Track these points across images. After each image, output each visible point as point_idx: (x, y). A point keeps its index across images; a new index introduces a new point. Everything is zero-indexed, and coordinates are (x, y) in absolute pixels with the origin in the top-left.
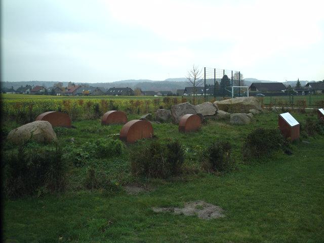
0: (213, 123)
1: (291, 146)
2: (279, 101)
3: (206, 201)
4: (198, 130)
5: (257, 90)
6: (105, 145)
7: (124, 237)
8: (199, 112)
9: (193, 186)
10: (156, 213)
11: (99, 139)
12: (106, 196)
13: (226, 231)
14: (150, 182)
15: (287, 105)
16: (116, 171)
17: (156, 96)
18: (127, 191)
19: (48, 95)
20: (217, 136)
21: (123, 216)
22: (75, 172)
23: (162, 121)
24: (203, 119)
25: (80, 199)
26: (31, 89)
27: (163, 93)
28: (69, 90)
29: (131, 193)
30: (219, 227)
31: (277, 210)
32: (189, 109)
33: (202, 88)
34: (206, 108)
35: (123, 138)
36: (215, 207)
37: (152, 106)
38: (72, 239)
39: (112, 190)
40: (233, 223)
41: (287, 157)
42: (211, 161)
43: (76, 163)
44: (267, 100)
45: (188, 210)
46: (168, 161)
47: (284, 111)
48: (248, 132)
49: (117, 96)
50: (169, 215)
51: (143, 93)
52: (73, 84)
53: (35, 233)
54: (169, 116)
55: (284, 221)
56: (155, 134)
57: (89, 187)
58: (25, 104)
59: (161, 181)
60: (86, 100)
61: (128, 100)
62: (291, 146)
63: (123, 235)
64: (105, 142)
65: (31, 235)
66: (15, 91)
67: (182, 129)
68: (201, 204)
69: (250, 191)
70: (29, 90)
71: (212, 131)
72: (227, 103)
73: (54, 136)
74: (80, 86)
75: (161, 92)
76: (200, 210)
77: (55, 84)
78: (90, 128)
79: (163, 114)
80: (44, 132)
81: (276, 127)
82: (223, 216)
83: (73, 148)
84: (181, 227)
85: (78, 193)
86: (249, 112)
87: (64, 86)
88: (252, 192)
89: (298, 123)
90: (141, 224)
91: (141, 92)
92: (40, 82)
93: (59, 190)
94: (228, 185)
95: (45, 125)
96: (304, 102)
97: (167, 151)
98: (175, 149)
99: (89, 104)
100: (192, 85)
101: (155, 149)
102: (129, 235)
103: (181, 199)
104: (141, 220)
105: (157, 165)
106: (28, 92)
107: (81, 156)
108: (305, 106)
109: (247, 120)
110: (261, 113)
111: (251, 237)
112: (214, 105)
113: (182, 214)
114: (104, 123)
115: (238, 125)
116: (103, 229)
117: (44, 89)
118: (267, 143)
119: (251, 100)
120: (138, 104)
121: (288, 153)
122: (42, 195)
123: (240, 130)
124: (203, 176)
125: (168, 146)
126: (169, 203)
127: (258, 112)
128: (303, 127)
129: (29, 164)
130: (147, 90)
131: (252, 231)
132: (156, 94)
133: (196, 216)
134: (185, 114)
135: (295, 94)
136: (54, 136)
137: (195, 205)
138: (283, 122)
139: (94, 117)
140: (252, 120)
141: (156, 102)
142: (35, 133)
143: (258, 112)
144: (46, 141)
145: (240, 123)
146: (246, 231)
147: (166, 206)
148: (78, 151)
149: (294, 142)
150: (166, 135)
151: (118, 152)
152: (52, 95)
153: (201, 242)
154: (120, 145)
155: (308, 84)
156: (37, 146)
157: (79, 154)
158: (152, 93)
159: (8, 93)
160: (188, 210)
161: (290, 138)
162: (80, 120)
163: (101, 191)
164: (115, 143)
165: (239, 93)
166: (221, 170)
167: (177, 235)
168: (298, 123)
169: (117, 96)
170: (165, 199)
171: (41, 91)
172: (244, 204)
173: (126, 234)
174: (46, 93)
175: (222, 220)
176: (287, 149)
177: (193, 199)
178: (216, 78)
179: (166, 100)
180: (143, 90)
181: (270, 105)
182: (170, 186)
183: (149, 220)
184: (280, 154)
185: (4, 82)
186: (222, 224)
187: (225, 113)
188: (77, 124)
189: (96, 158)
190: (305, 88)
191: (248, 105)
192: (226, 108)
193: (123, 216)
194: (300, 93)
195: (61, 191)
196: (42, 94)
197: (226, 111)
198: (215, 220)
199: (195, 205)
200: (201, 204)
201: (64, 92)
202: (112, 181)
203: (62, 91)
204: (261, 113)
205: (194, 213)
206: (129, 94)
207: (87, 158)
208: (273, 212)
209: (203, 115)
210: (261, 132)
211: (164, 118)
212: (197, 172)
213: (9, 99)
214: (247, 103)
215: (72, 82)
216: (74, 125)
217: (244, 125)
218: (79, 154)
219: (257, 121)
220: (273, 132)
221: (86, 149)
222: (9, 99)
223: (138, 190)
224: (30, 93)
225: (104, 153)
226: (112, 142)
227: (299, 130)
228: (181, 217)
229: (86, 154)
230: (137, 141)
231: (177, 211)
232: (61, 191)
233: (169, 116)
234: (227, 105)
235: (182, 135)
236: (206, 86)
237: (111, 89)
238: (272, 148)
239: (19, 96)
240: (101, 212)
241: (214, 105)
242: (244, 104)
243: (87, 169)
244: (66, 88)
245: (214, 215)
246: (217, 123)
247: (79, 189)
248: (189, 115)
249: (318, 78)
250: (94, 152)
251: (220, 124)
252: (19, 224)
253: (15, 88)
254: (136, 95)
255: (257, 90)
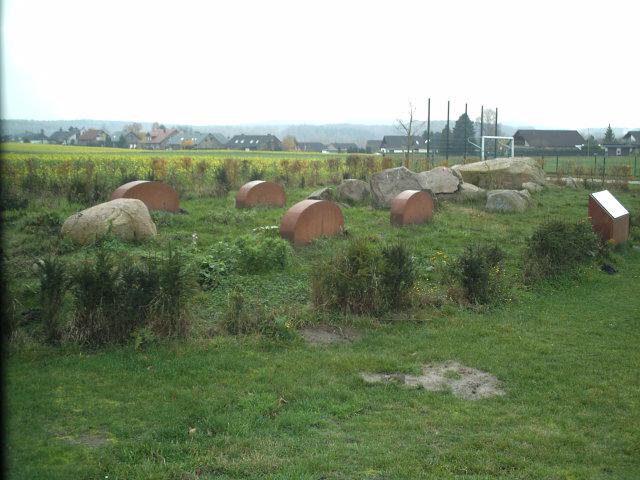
0: (453, 208)
1: (614, 256)
2: (576, 166)
3: (465, 362)
4: (427, 221)
5: (527, 145)
6: (255, 248)
7: (314, 429)
8: (426, 186)
9: (434, 332)
10: (370, 385)
11: (243, 237)
12: (267, 348)
13: (511, 423)
14: (350, 322)
15: (592, 174)
16: (283, 300)
17: (324, 152)
18: (306, 339)
19: (112, 147)
20: (467, 234)
21: (305, 388)
22: (201, 300)
23: (351, 202)
24: (435, 200)
25: (217, 353)
26: (78, 135)
27: (339, 147)
28: (153, 138)
29: (314, 344)
30: (497, 415)
31: (605, 383)
32: (408, 181)
33: (418, 138)
34: (441, 176)
35: (286, 234)
36: (483, 375)
37: (324, 172)
38: (214, 433)
39: (277, 338)
40: (523, 408)
41: (605, 277)
42: (466, 283)
43: (201, 283)
44: (551, 163)
45: (431, 379)
46: (385, 282)
47: (599, 188)
48: (529, 230)
49: (247, 150)
50: (396, 389)
51: (301, 146)
52: (162, 127)
53: (142, 419)
54: (366, 194)
55: (621, 406)
56: (348, 227)
57: (232, 330)
58: (78, 165)
59: (372, 320)
60: (196, 159)
61: (279, 160)
62: (614, 256)
63: (312, 425)
64: (255, 241)
65: (135, 422)
66: (46, 138)
67: (397, 219)
68: (454, 367)
69: (548, 345)
70: (74, 137)
71: (455, 224)
72: (478, 169)
73: (152, 229)
74: (176, 132)
75: (335, 145)
76: (452, 379)
77: (126, 126)
78: (218, 214)
79: (353, 189)
80: (133, 220)
81: (583, 216)
82: (501, 393)
83: (197, 255)
84: (423, 412)
85: (213, 341)
86: (521, 189)
87: (144, 130)
88: (551, 345)
89: (627, 212)
90: (346, 406)
91: (297, 144)
92: (97, 121)
93: (175, 335)
94: (503, 331)
95: (135, 207)
96: (626, 170)
97: (382, 263)
98: (397, 257)
99: (202, 167)
100: (406, 133)
101: (357, 259)
102: (324, 426)
103: (415, 357)
104: (343, 399)
105: (363, 289)
106: (73, 141)
107: (211, 269)
108: (628, 177)
109: (521, 204)
110: (545, 190)
111: (564, 436)
112: (454, 173)
113: (420, 388)
114: (241, 204)
115: (503, 213)
116: (271, 413)
117: (104, 136)
118: (570, 251)
119: (527, 164)
120: (297, 167)
121: (607, 269)
122: (145, 345)
123: (507, 222)
124: (450, 313)
125: (383, 253)
126: (392, 365)
127: (539, 188)
128: (633, 219)
129: (117, 283)
130: (308, 141)
131: (563, 425)
132: (326, 148)
133: (448, 392)
134: (403, 189)
135: (602, 153)
136: (152, 229)
137: (444, 370)
138: (596, 208)
139: (217, 192)
140: (529, 205)
141: (333, 164)
142: (116, 222)
143: (539, 188)
144: (137, 239)
145: (506, 208)
146: (552, 425)
147: (387, 372)
148: (204, 258)
149: (618, 249)
150: (375, 235)
151: (280, 262)
152: (107, 146)
153: (122, 477)
154: (284, 248)
155: (629, 135)
156: (122, 247)
157: (207, 265)
158: (317, 147)
159: (33, 142)
160: (431, 379)
161: (611, 240)
162: (190, 198)
163: (256, 338)
164: (275, 245)
165: (494, 151)
166: (484, 301)
167: (417, 428)
168: (627, 212)
169: (247, 150)
170: (383, 356)
171: (98, 139)
172: (538, 370)
173: (318, 425)
174: (108, 143)
175: (500, 401)
176: (607, 262)
177: (439, 359)
178: (431, 120)
179: (352, 161)
180: (299, 141)
181: (559, 174)
182: (388, 332)
183: (358, 398)
184: (593, 271)
185: (10, 121)
186: (502, 409)
187: (475, 189)
188: (188, 206)
189: (240, 273)
190: (623, 141)
191: (519, 175)
192: (475, 178)
193: (305, 388)
194: (612, 150)
195: (179, 337)
196: (100, 144)
197: (476, 183)
198: (487, 401)
199: (444, 370)
200: (454, 367)
201: (144, 141)
202: (278, 320)
203: (140, 139)
204: (545, 190)
205: (444, 386)
206: (273, 146)
207: (222, 273)
208: (598, 387)
209: (435, 191)
210: (559, 228)
211: (355, 197)
212: (438, 304)
213: (17, 152)
214: (517, 170)
215: (160, 123)
216: (181, 206)
217: (514, 213)
218: (207, 265)
219: (540, 205)
220: (579, 228)
221: (219, 256)
222: (17, 152)
223: (327, 338)
224: (76, 142)
225: (253, 265)
226: (269, 244)
227: (627, 226)
228: (419, 393)
229: (221, 266)
230: (314, 243)
231: (410, 381)
232: (179, 337)
233: (366, 194)
234: (477, 172)
235: (397, 231)
236: (427, 135)
237: (236, 137)
238: (578, 259)
239: (54, 147)
240: (261, 380)
241: (454, 173)
242: (511, 171)
243: (230, 294)
244: (148, 135)
245: (484, 391)
246: (462, 209)
247: (212, 334)
248: (411, 192)
249: (624, 124)
250: (234, 260)
251: (467, 210)
252: (107, 401)
253: (48, 133)
254: (287, 149)
255: (527, 145)
